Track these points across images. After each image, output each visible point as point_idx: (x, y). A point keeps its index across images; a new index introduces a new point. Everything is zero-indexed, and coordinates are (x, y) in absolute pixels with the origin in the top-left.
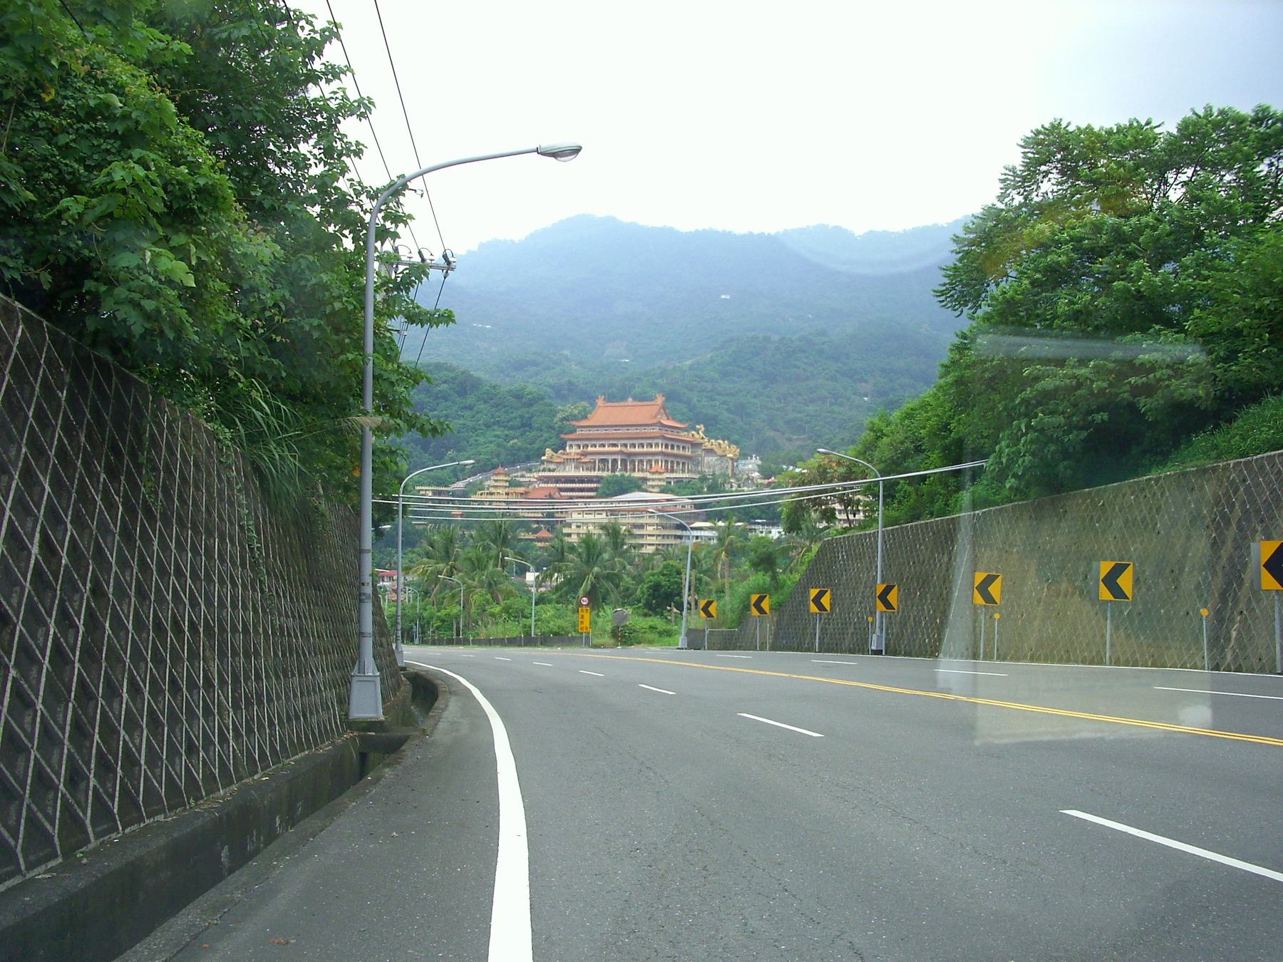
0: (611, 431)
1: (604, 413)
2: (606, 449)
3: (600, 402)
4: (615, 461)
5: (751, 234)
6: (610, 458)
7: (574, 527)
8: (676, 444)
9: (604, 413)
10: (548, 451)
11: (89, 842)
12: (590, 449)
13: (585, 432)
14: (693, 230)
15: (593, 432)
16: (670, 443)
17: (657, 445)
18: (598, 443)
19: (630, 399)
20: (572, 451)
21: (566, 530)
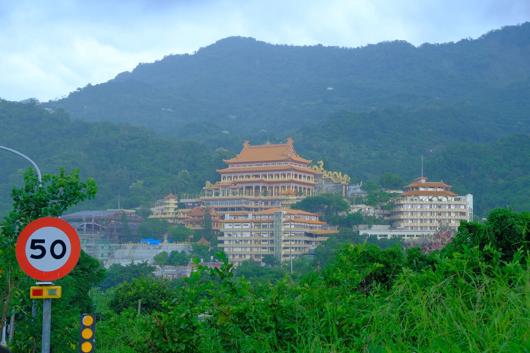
0: (254, 167)
1: (249, 152)
2: (251, 179)
3: (246, 145)
4: (257, 188)
5: (286, 45)
6: (254, 185)
7: (226, 236)
8: (303, 174)
9: (249, 152)
10: (208, 183)
11: (33, 295)
12: (239, 179)
13: (235, 167)
14: (394, 40)
15: (241, 167)
16: (298, 174)
17: (289, 174)
18: (245, 174)
19: (268, 143)
20: (225, 181)
21: (219, 238)
